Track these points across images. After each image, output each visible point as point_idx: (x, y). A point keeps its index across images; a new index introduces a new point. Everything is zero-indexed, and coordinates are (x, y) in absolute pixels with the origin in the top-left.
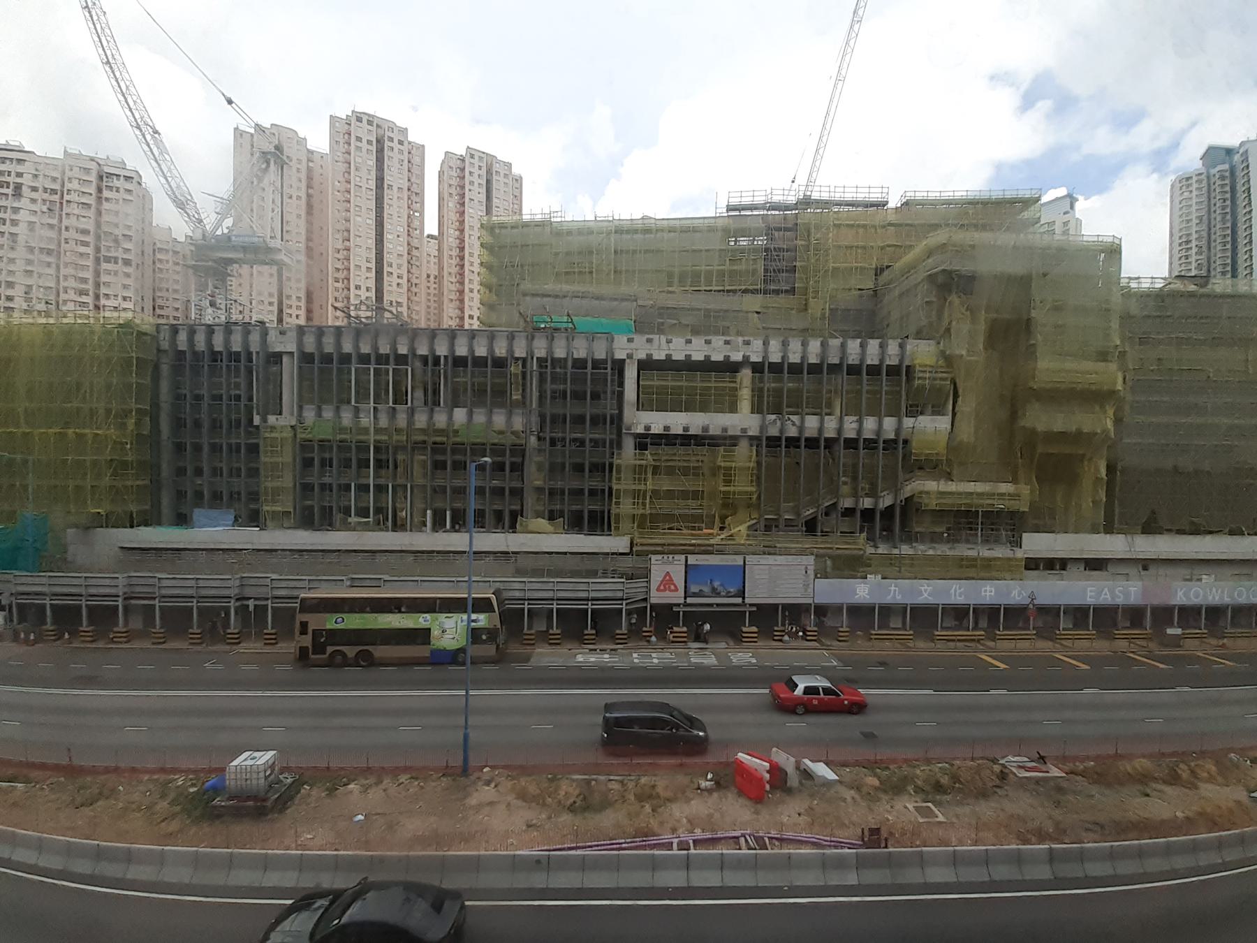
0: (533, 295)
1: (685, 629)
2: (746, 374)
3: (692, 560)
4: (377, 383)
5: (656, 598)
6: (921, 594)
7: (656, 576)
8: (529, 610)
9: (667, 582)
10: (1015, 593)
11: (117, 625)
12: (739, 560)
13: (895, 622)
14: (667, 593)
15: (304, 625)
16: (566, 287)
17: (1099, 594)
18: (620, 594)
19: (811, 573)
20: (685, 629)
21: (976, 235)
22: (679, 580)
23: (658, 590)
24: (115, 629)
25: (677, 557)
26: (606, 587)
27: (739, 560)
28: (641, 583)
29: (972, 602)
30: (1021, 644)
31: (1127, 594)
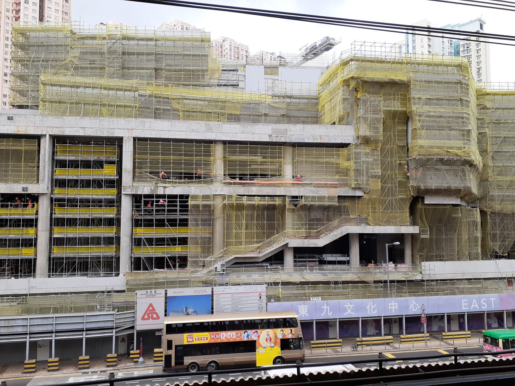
0: (52, 85)
1: (88, 357)
2: (218, 151)
3: (171, 292)
4: (279, 184)
5: (141, 325)
6: (345, 310)
7: (141, 309)
8: (30, 342)
9: (151, 312)
10: (411, 306)
11: (111, 353)
12: (207, 291)
13: (42, 355)
14: (151, 321)
15: (170, 343)
16: (79, 80)
17: (470, 304)
18: (109, 325)
19: (264, 298)
20: (469, 332)
21: (120, 84)
22: (160, 309)
23: (143, 319)
24: (109, 355)
25: (158, 291)
26: (103, 318)
27: (207, 291)
28: (128, 314)
29: (404, 314)
30: (416, 344)
31: (489, 303)
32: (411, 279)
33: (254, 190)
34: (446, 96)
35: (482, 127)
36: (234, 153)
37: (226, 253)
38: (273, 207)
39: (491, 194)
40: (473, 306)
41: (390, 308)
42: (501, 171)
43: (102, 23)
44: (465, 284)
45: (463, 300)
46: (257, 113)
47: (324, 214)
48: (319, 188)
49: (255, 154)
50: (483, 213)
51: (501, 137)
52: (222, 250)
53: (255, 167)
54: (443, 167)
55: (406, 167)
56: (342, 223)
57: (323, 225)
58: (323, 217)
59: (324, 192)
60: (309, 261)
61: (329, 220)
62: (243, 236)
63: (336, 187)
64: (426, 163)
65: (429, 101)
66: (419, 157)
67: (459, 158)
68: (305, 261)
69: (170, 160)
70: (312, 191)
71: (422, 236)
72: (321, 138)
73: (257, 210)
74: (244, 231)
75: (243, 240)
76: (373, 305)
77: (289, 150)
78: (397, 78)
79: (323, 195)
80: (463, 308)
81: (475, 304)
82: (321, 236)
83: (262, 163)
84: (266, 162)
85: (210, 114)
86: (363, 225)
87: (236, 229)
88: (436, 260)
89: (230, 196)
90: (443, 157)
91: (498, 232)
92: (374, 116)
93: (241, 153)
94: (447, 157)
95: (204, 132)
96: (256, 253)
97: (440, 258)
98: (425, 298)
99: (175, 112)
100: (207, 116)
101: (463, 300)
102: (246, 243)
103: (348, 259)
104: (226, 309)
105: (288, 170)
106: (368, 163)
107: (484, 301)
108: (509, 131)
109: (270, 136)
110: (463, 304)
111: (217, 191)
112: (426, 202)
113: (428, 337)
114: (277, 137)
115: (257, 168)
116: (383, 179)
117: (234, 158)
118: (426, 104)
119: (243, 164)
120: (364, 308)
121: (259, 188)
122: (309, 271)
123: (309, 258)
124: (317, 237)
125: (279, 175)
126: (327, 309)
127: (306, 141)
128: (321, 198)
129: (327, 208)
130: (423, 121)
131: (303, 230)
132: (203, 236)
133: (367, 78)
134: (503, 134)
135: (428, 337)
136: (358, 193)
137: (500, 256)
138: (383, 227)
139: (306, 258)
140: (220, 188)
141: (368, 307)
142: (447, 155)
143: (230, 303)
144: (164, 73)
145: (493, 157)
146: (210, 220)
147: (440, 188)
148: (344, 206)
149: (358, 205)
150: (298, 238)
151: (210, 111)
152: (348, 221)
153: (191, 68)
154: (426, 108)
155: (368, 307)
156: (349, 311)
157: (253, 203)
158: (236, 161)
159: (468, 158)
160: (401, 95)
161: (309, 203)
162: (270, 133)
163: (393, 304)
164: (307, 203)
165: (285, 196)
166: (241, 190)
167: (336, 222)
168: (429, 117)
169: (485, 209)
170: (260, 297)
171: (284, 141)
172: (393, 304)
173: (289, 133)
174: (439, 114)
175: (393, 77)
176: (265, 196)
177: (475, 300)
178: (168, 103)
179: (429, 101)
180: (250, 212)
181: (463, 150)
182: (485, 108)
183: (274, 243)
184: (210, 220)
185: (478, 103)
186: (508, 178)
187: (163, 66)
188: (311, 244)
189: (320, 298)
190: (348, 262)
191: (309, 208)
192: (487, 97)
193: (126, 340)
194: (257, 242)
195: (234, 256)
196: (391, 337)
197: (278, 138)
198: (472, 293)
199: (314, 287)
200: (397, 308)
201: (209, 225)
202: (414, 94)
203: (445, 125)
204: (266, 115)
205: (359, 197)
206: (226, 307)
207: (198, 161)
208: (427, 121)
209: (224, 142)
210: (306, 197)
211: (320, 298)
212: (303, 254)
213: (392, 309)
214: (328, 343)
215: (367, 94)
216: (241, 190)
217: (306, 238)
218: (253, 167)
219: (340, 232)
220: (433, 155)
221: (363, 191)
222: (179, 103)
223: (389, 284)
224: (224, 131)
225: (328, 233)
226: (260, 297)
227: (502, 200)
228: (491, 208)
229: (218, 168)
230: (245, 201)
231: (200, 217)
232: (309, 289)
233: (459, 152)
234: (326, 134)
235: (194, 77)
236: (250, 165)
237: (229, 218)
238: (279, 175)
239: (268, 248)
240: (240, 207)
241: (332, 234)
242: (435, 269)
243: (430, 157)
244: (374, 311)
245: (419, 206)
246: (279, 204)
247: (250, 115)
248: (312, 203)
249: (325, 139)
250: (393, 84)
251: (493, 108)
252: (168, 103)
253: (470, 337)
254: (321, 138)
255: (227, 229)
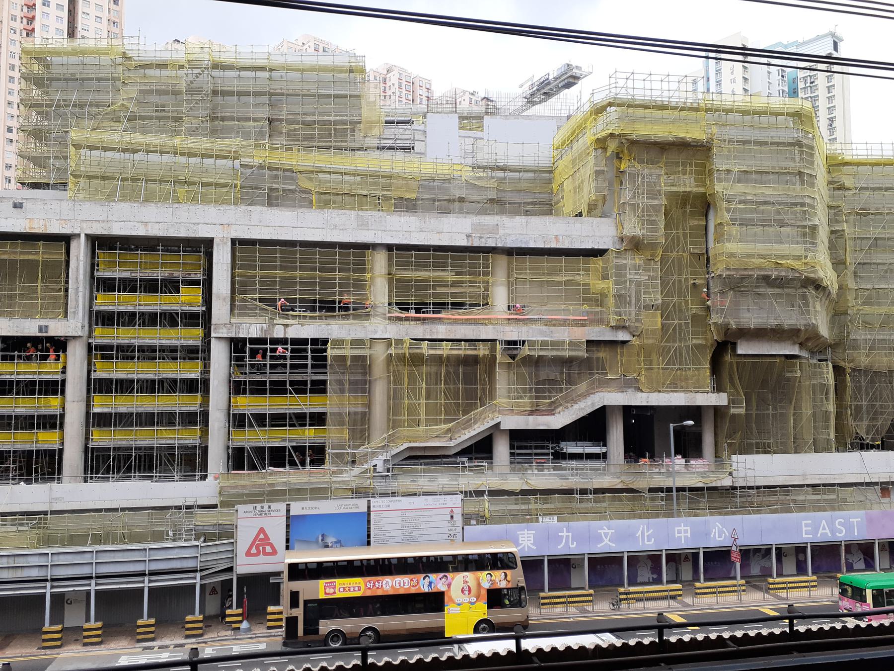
0: (90, 148)
1: (152, 621)
2: (379, 262)
3: (297, 508)
4: (484, 319)
5: (246, 565)
6: (599, 539)
7: (244, 538)
8: (53, 595)
9: (262, 543)
10: (714, 533)
11: (193, 613)
12: (360, 505)
13: (73, 617)
14: (261, 558)
15: (295, 596)
16: (137, 138)
17: (816, 529)
18: (189, 564)
19: (458, 517)
20: (815, 578)
22: (278, 537)
23: (248, 554)
24: (189, 618)
25: (274, 506)
26: (179, 553)
27: (360, 505)
28: (221, 546)
29: (701, 545)
30: (722, 598)
31: (849, 527)
32: (714, 485)
33: (441, 331)
34: (773, 168)
35: (837, 221)
36: (405, 266)
37: (392, 440)
38: (474, 360)
39: (852, 337)
40: (821, 531)
41: (677, 535)
42: (869, 297)
43: (176, 40)
44: (807, 493)
45: (804, 522)
46: (446, 197)
47: (562, 373)
48: (554, 326)
49: (443, 267)
50: (838, 370)
51: (870, 238)
52: (385, 435)
53: (443, 290)
54: (769, 290)
55: (705, 290)
56: (593, 388)
57: (561, 390)
58: (561, 377)
59: (563, 334)
60: (536, 454)
61: (570, 382)
62: (422, 410)
63: (583, 325)
64: (740, 284)
65: (744, 176)
66: (728, 273)
67: (797, 275)
68: (530, 454)
69: (296, 278)
70: (542, 333)
71: (733, 411)
72: (557, 241)
73: (446, 365)
74: (423, 402)
75: (423, 417)
76: (648, 531)
77: (502, 261)
78: (688, 136)
79: (561, 339)
80: (804, 536)
81: (824, 529)
82: (557, 411)
83: (455, 284)
84: (462, 282)
85: (364, 199)
86: (630, 391)
87: (409, 398)
88: (758, 453)
89: (399, 342)
90: (770, 273)
91: (864, 403)
92: (650, 201)
93: (419, 266)
94: (776, 273)
95: (353, 229)
96: (445, 439)
97: (764, 449)
98: (738, 517)
99: (304, 195)
100: (359, 201)
101: (804, 522)
102: (428, 422)
103: (604, 449)
104: (393, 537)
105: (500, 296)
106: (638, 283)
107: (840, 523)
108: (884, 227)
109: (468, 236)
110: (804, 529)
111: (376, 332)
112: (740, 351)
113: (743, 585)
114: (481, 237)
115: (447, 293)
116: (665, 310)
117: (406, 274)
118: (739, 181)
119: (422, 284)
120: (632, 536)
121: (449, 327)
122: (536, 471)
123: (536, 448)
124: (551, 412)
125: (483, 305)
126: (568, 537)
127: (532, 245)
128: (557, 345)
129: (568, 362)
130: (735, 210)
131: (526, 400)
132: (353, 410)
133: (637, 135)
134: (874, 233)
135: (743, 585)
136: (622, 336)
137: (868, 444)
138: (666, 395)
139: (531, 448)
140: (381, 327)
141: (640, 533)
142: (776, 270)
143: (399, 527)
144: (284, 128)
145: (855, 273)
146: (365, 382)
147: (764, 326)
148: (598, 358)
149: (622, 356)
150: (517, 414)
151: (364, 192)
152: (605, 384)
153: (332, 118)
154: (740, 188)
155: (640, 533)
156: (606, 541)
157: (439, 352)
158: (410, 281)
159: (812, 275)
160: (696, 165)
161: (536, 354)
162: (469, 231)
163: (682, 528)
164: (533, 353)
165: (495, 340)
166: (419, 331)
167: (583, 387)
168: (745, 203)
169: (842, 364)
170: (452, 517)
171: (494, 245)
172: (682, 528)
173: (501, 232)
174: (761, 199)
175: (682, 134)
176: (460, 340)
177: (824, 522)
178: (292, 179)
179: (744, 176)
180: (433, 369)
181: (804, 261)
182: (841, 187)
183: (475, 423)
184: (365, 382)
185: (830, 179)
186: (883, 310)
187: (283, 114)
188: (539, 425)
189: (556, 518)
190: (604, 456)
191: (536, 362)
192: (846, 169)
193: (219, 592)
194: (447, 421)
195: (406, 446)
196: (679, 586)
197: (482, 240)
198: (820, 509)
199: (545, 499)
200: (689, 535)
201: (363, 391)
202: (719, 163)
203: (773, 217)
204: (461, 200)
205: (624, 342)
206: (393, 533)
207: (344, 279)
208: (741, 211)
209: (389, 247)
210: (532, 343)
211: (556, 518)
212: (525, 442)
213: (680, 537)
214: (570, 596)
215: (636, 164)
216: (419, 331)
217: (532, 413)
218: (439, 290)
219: (589, 403)
220: (752, 269)
221: (630, 333)
222: (310, 179)
223: (674, 493)
224: (388, 228)
225: (569, 405)
226: (452, 517)
227: (871, 348)
228: (852, 361)
229: (379, 292)
230: (425, 349)
231: (346, 378)
232: (536, 503)
233: (797, 265)
234: (567, 233)
235: (337, 134)
236: (434, 287)
237: (397, 379)
238: (483, 305)
239: (466, 431)
240: (416, 360)
241: (576, 407)
242: (755, 468)
243: (746, 273)
244: (649, 540)
245: (728, 358)
246: (484, 355)
247: (434, 200)
248: (542, 353)
249: (563, 242)
250: (682, 145)
251: (856, 188)
252: (292, 179)
253: (815, 586)
254: (557, 241)
255: (395, 398)
